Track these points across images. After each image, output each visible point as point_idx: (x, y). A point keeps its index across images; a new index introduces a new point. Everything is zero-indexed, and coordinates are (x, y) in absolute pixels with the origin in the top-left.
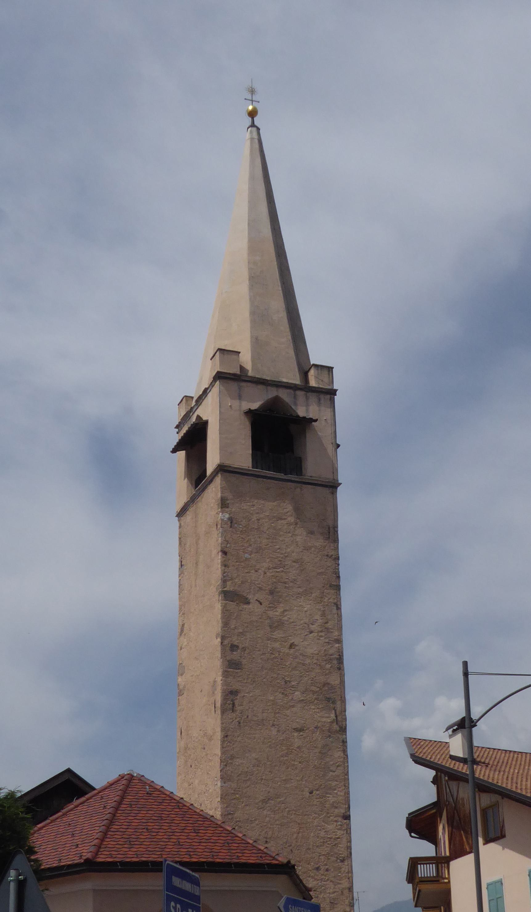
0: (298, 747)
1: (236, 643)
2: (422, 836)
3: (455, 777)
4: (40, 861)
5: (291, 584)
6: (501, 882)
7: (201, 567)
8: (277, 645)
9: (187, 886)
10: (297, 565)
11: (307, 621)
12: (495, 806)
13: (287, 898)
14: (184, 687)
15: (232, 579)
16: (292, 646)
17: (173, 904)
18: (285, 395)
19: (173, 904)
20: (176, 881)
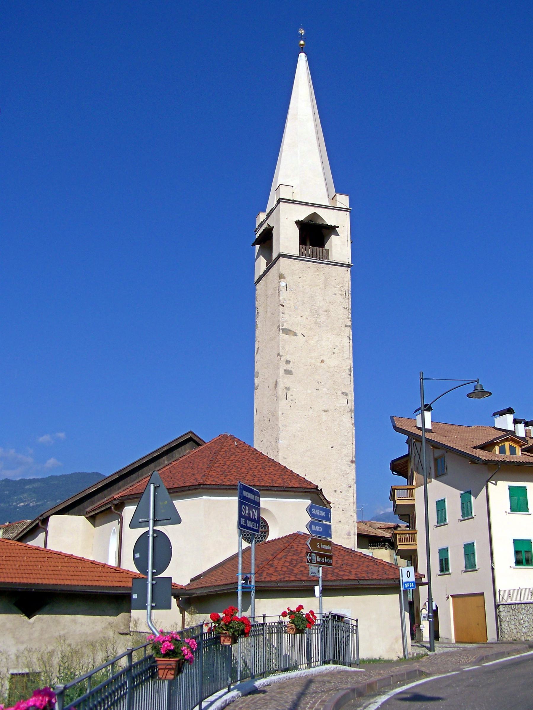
0: (325, 421)
1: (289, 360)
2: (400, 474)
3: (418, 438)
4: (144, 683)
5: (322, 325)
6: (444, 500)
7: (269, 314)
8: (313, 361)
9: (252, 497)
10: (326, 313)
11: (331, 347)
12: (443, 457)
13: (191, 437)
14: (258, 385)
15: (287, 321)
16: (322, 361)
17: (243, 506)
18: (320, 212)
19: (243, 506)
20: (246, 494)
